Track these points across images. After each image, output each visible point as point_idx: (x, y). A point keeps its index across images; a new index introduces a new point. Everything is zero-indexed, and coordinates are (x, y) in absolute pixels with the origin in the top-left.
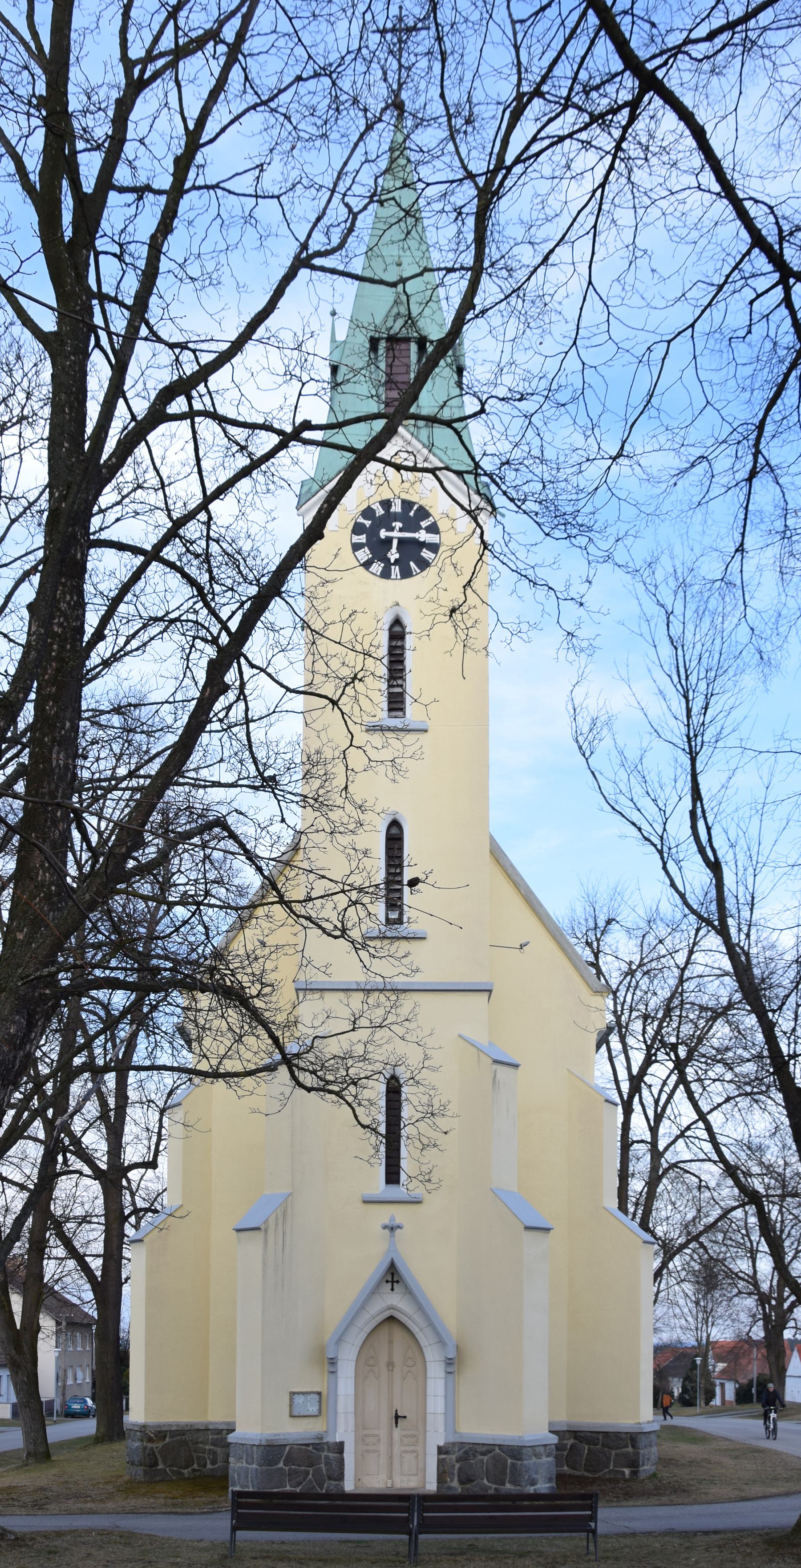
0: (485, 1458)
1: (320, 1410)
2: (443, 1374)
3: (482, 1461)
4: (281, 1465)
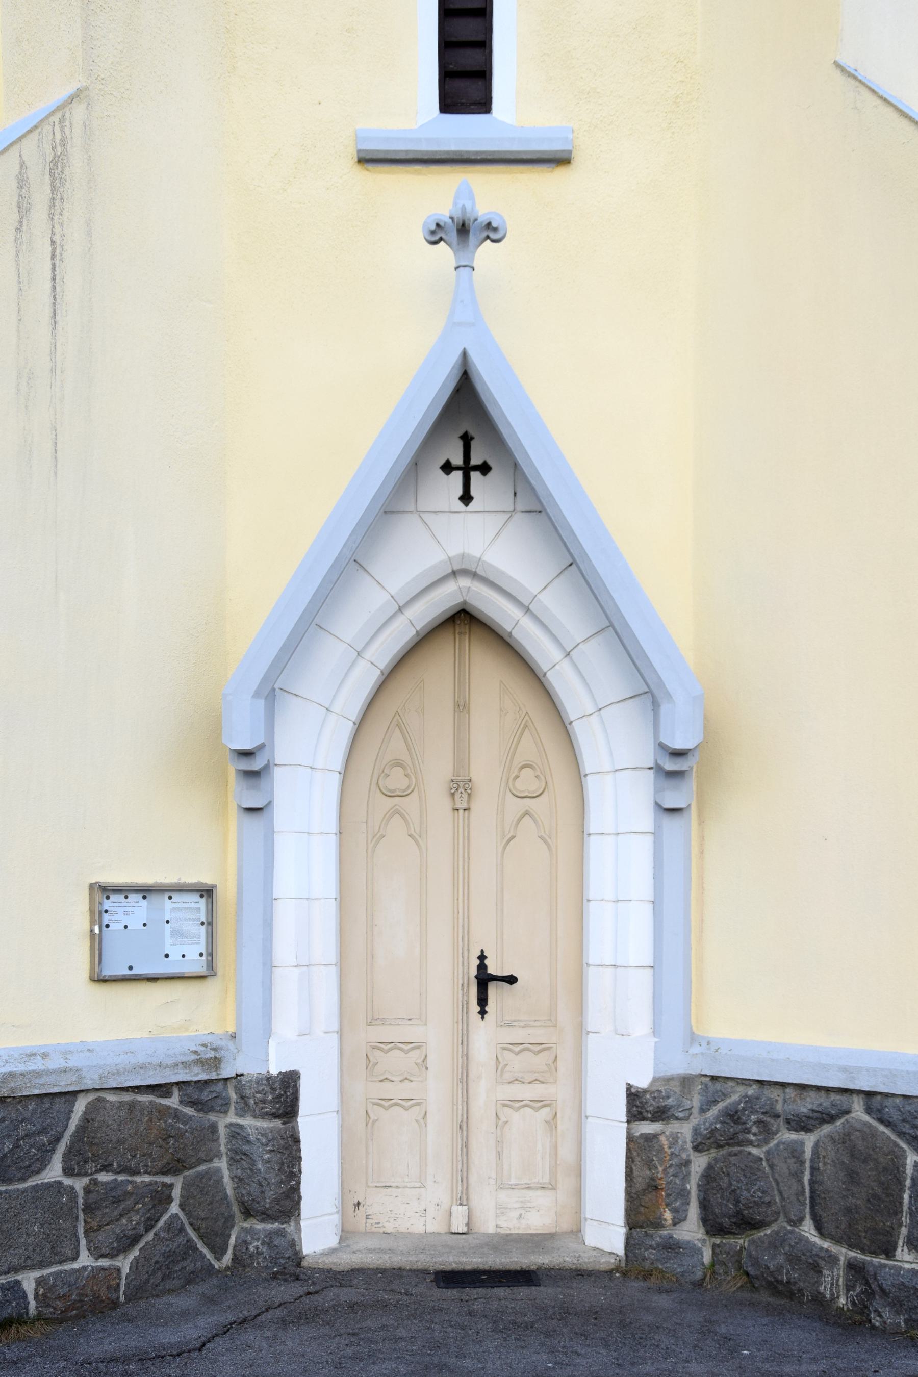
0: (809, 1141)
1: (210, 954)
2: (645, 819)
3: (795, 1151)
4: (54, 1172)
